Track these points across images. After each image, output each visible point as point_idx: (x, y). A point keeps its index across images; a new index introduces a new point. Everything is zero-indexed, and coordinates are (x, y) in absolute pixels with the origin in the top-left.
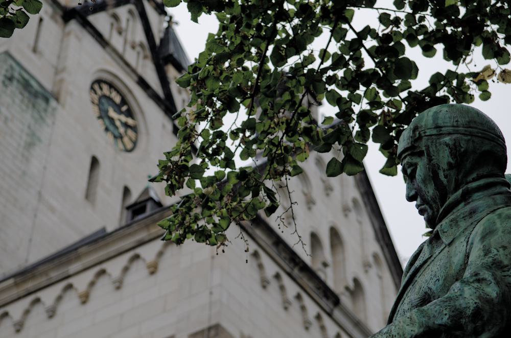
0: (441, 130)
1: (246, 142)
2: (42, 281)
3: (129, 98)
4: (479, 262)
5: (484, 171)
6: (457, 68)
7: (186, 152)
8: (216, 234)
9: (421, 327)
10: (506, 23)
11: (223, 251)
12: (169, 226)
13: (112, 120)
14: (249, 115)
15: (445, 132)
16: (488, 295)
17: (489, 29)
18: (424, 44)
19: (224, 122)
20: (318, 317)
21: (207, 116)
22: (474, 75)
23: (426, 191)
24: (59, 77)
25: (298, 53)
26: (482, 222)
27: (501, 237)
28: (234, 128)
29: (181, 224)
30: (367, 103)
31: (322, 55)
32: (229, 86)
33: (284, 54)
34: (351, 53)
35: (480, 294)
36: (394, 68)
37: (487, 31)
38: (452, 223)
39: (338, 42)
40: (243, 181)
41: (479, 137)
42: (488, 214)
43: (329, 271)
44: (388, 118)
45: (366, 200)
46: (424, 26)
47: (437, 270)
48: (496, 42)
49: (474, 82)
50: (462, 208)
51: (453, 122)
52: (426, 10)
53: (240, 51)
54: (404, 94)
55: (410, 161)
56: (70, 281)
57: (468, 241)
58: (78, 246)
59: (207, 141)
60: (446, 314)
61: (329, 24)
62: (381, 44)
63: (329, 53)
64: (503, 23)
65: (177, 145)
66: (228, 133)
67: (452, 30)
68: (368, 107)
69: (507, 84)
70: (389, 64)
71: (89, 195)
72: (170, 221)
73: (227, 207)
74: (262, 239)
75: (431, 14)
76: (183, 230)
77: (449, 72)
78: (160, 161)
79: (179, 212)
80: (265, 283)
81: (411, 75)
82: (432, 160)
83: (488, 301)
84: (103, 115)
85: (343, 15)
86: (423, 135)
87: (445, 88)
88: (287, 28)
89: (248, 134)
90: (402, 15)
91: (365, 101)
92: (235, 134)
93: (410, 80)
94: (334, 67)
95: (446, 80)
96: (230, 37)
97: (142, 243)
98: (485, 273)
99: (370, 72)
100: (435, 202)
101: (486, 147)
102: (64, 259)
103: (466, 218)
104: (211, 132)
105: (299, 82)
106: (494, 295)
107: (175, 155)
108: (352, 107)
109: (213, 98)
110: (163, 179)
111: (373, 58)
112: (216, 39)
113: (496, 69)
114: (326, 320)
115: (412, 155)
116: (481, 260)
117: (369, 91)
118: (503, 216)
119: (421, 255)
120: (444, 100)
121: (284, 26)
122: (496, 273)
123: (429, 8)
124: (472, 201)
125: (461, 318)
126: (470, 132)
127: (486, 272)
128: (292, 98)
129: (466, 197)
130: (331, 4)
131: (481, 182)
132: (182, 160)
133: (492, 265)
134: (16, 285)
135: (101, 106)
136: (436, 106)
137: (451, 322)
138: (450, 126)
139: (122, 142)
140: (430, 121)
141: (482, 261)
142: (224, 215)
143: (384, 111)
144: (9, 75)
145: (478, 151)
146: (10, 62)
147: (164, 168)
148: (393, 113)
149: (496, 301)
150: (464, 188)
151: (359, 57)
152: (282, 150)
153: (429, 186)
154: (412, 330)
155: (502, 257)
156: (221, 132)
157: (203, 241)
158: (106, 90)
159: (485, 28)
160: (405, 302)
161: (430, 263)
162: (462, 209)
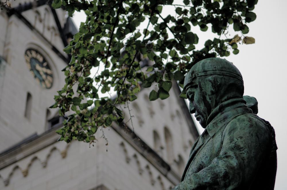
0: (207, 73)
3: (47, 58)
4: (227, 146)
5: (230, 95)
6: (220, 37)
7: (70, 90)
8: (89, 136)
9: (195, 184)
10: (245, 11)
11: (93, 146)
12: (63, 133)
13: (38, 72)
15: (208, 74)
16: (232, 165)
17: (237, 14)
18: (201, 24)
20: (159, 178)
22: (229, 41)
23: (200, 107)
27: (239, 131)
28: (97, 75)
29: (69, 131)
30: (170, 59)
31: (145, 32)
32: (93, 52)
34: (161, 31)
35: (227, 164)
36: (185, 38)
38: (214, 125)
39: (153, 24)
40: (104, 105)
42: (233, 119)
44: (183, 67)
46: (201, 14)
47: (206, 152)
48: (241, 21)
49: (230, 44)
50: (219, 116)
51: (213, 68)
52: (201, 5)
53: (100, 31)
54: (191, 53)
55: (191, 91)
57: (222, 135)
59: (82, 84)
60: (209, 177)
61: (149, 14)
62: (177, 25)
64: (244, 10)
66: (94, 79)
67: (216, 16)
68: (171, 61)
69: (248, 45)
70: (182, 36)
71: (27, 114)
73: (95, 120)
75: (204, 7)
77: (215, 39)
82: (202, 90)
83: (232, 168)
84: (33, 69)
85: (156, 9)
86: (197, 76)
87: (214, 48)
88: (124, 18)
89: (105, 78)
90: (188, 8)
91: (169, 57)
92: (97, 79)
93: (194, 44)
94: (151, 39)
95: (214, 44)
97: (56, 141)
98: (230, 152)
99: (172, 41)
100: (205, 113)
101: (232, 82)
103: (222, 121)
104: (84, 78)
105: (133, 48)
106: (235, 164)
107: (64, 92)
109: (84, 59)
110: (57, 106)
112: (85, 25)
113: (241, 36)
114: (164, 179)
115: (191, 87)
116: (229, 145)
118: (241, 119)
119: (198, 143)
120: (213, 55)
122: (236, 152)
124: (225, 112)
125: (218, 178)
126: (223, 73)
127: (231, 152)
129: (221, 110)
130: (149, 3)
131: (230, 101)
132: (68, 95)
133: (234, 148)
136: (204, 60)
137: (212, 180)
138: (211, 71)
140: (201, 68)
141: (229, 146)
145: (227, 84)
147: (58, 100)
149: (236, 168)
150: (220, 105)
151: (165, 32)
154: (191, 187)
155: (240, 143)
157: (82, 140)
158: (34, 54)
159: (234, 14)
160: (190, 170)
161: (203, 148)
162: (220, 117)
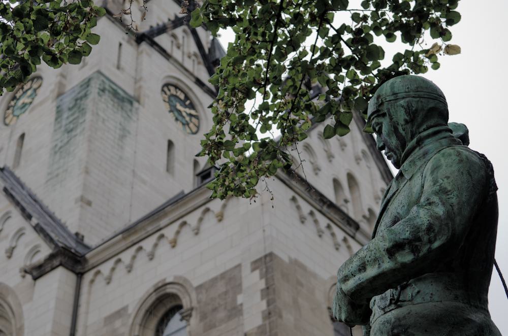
1: (263, 120)
2: (142, 234)
3: (190, 95)
4: (430, 191)
6: (413, 48)
10: (445, 11)
11: (255, 202)
12: (214, 187)
13: (179, 112)
14: (264, 99)
17: (434, 16)
18: (387, 32)
19: (245, 107)
20: (345, 240)
21: (232, 104)
22: (426, 52)
24: (138, 85)
25: (295, 50)
26: (431, 160)
28: (253, 110)
29: (223, 185)
30: (349, 81)
33: (284, 52)
34: (334, 46)
37: (433, 18)
39: (323, 38)
41: (425, 98)
43: (350, 205)
44: (365, 91)
45: (372, 150)
46: (385, 20)
49: (426, 57)
52: (386, 7)
53: (253, 53)
55: (377, 121)
56: (162, 232)
58: (165, 206)
61: (316, 26)
62: (355, 36)
63: (317, 47)
65: (213, 128)
66: (250, 115)
70: (362, 50)
71: (169, 168)
72: (215, 184)
74: (298, 188)
76: (225, 189)
77: (407, 51)
78: (201, 141)
79: (221, 177)
80: (303, 220)
81: (379, 57)
82: (393, 119)
83: (438, 218)
84: (173, 109)
86: (384, 101)
87: (405, 64)
88: (284, 33)
89: (264, 113)
90: (368, 13)
91: (347, 80)
92: (254, 115)
94: (322, 57)
95: (405, 58)
96: (243, 44)
102: (156, 217)
105: (298, 71)
106: (441, 213)
108: (338, 85)
110: (205, 154)
111: (350, 47)
114: (351, 242)
115: (378, 116)
117: (349, 72)
118: (446, 154)
120: (406, 72)
121: (283, 31)
123: (388, 5)
124: (425, 146)
125: (419, 232)
128: (294, 84)
129: (419, 143)
134: (124, 238)
135: (171, 103)
139: (189, 127)
140: (389, 91)
142: (253, 174)
143: (362, 86)
144: (101, 88)
145: (426, 109)
146: (102, 78)
147: (205, 145)
148: (369, 87)
149: (443, 217)
151: (339, 47)
152: (290, 123)
153: (392, 138)
156: (244, 114)
159: (430, 16)
162: (418, 152)
